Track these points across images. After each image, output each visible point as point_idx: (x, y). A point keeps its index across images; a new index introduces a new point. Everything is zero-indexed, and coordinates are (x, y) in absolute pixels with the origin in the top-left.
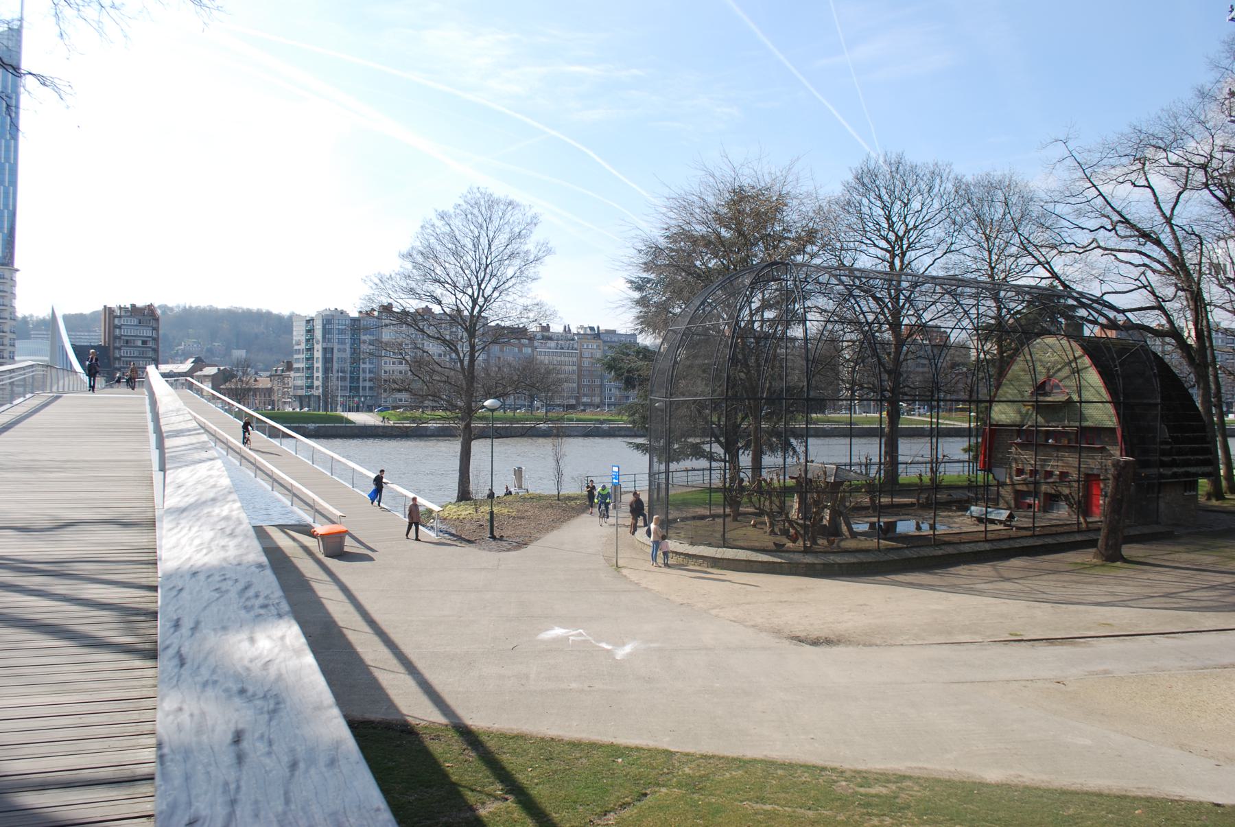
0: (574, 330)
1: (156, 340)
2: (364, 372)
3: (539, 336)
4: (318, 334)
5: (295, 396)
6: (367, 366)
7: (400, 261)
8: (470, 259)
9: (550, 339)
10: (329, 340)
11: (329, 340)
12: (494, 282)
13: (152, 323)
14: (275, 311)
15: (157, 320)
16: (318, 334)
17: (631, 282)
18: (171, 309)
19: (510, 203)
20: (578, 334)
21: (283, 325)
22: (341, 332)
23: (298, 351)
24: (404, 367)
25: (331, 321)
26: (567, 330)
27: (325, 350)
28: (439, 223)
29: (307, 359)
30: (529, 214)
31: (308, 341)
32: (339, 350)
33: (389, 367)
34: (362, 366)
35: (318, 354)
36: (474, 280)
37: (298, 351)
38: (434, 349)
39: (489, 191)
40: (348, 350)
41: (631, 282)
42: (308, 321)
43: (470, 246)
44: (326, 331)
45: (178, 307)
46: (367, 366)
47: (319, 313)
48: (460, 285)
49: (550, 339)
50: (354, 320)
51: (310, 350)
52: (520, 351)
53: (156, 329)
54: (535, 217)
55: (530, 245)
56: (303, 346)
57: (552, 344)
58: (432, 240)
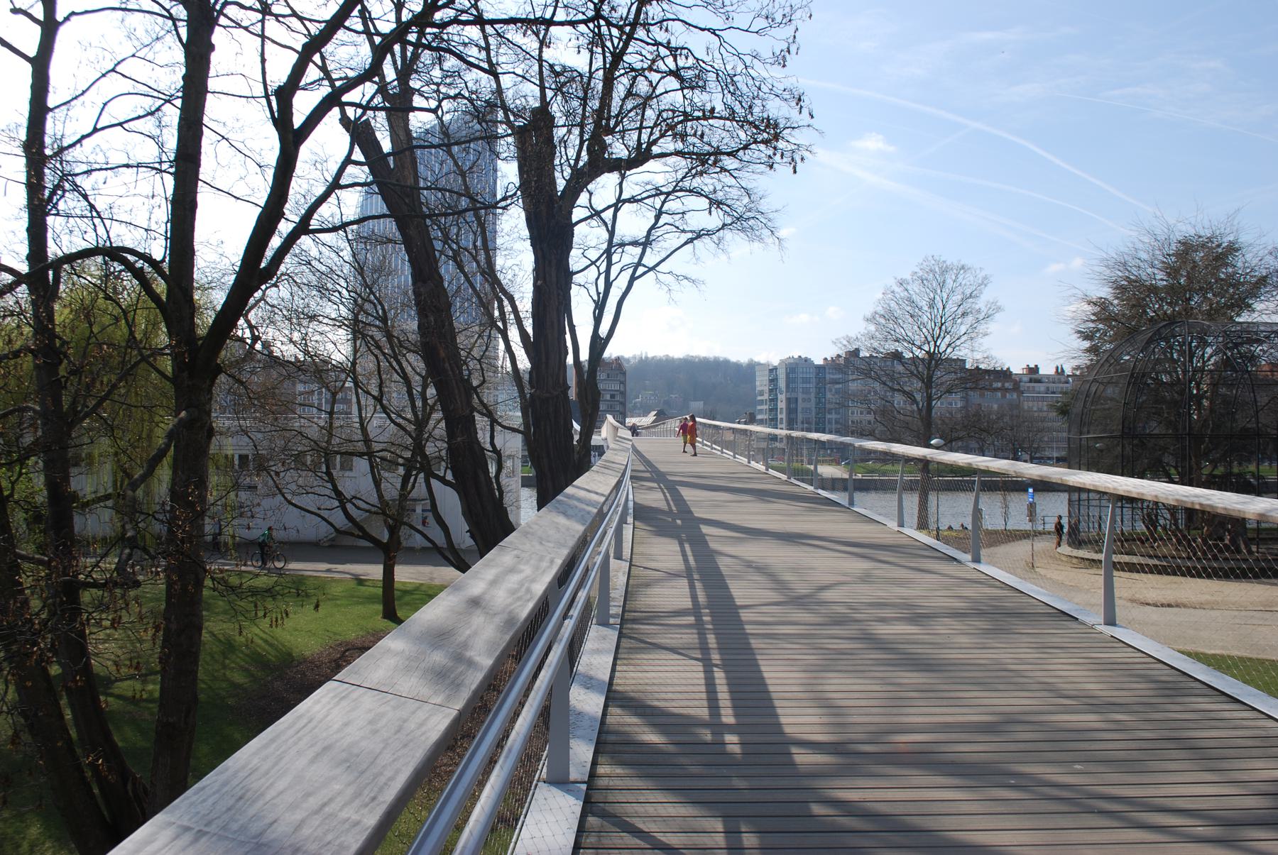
0: (1068, 371)
1: (623, 394)
2: (830, 422)
3: (1025, 379)
4: (782, 383)
5: (759, 449)
6: (834, 416)
7: (864, 324)
8: (925, 319)
9: (1039, 381)
10: (794, 390)
11: (794, 390)
12: (947, 340)
13: (620, 377)
14: (733, 359)
15: (624, 374)
16: (782, 383)
17: (1079, 332)
18: (628, 360)
19: (963, 268)
20: (1074, 375)
21: (746, 373)
22: (806, 380)
23: (761, 402)
24: (871, 417)
25: (796, 369)
26: (1060, 372)
27: (789, 400)
28: (897, 289)
29: (771, 410)
30: (980, 276)
31: (771, 391)
32: (804, 400)
33: (856, 417)
34: (828, 416)
35: (782, 405)
36: (930, 339)
37: (761, 402)
38: (899, 400)
39: (943, 259)
40: (813, 400)
41: (1079, 332)
42: (771, 371)
43: (926, 308)
44: (789, 381)
45: (634, 357)
46: (834, 416)
47: (782, 361)
48: (918, 343)
49: (1039, 381)
50: (819, 367)
51: (774, 400)
52: (1004, 396)
53: (623, 383)
54: (985, 278)
55: (981, 304)
56: (766, 397)
57: (1042, 387)
58: (893, 304)
